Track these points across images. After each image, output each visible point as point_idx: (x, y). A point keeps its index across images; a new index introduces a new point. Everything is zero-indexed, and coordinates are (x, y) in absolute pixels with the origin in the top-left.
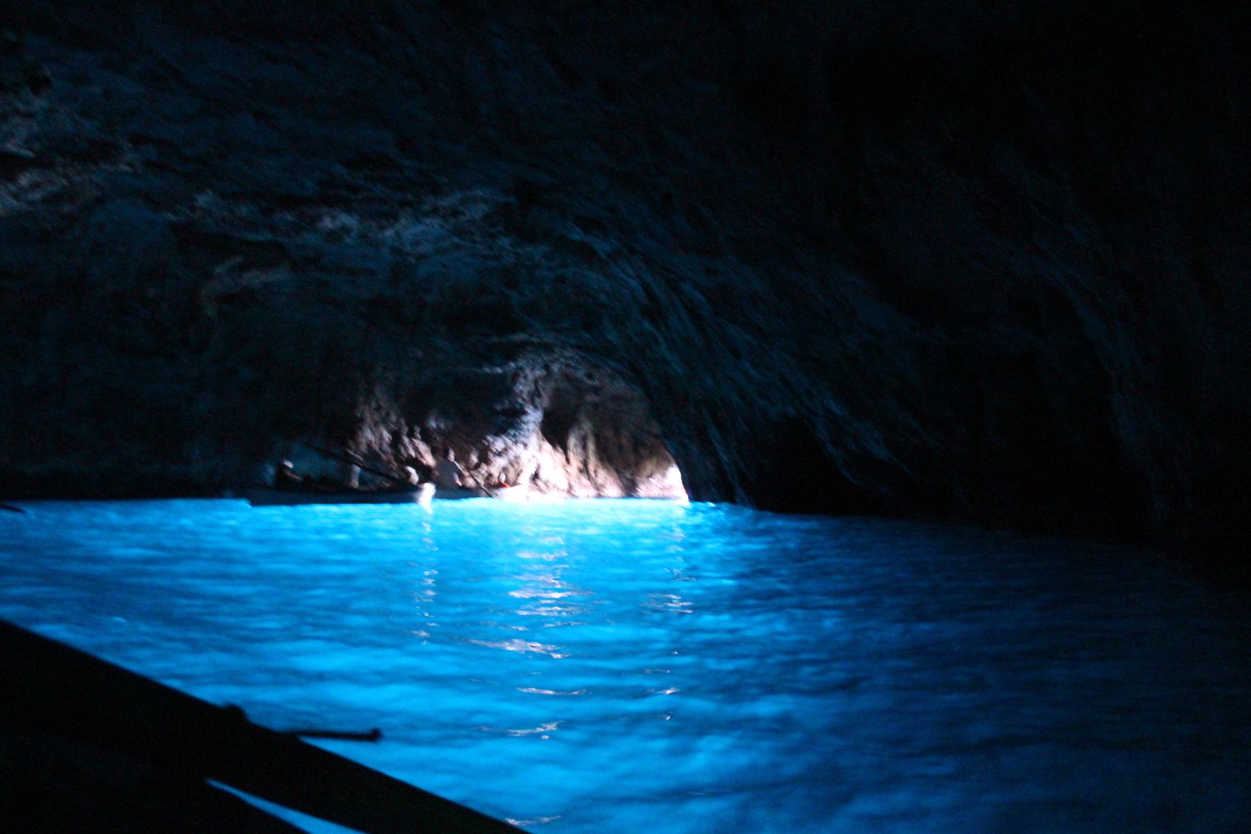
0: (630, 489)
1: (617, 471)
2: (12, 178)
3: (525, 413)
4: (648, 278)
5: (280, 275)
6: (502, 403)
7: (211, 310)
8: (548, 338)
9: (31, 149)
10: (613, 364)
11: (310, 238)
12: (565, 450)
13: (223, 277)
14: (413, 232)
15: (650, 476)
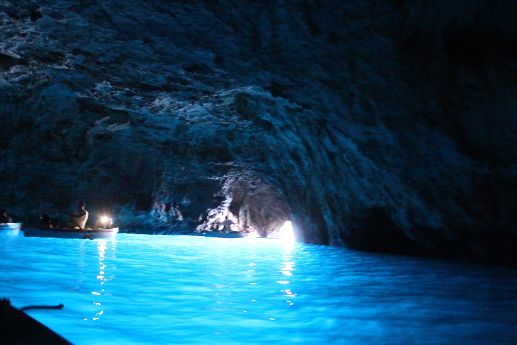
0: (264, 235)
1: (259, 226)
2: (7, 68)
3: (225, 199)
4: (308, 138)
5: (124, 127)
6: (217, 194)
7: (91, 142)
8: (242, 165)
9: (20, 54)
10: (270, 178)
11: (144, 110)
12: (238, 217)
13: (100, 125)
14: (194, 111)
15: (273, 230)
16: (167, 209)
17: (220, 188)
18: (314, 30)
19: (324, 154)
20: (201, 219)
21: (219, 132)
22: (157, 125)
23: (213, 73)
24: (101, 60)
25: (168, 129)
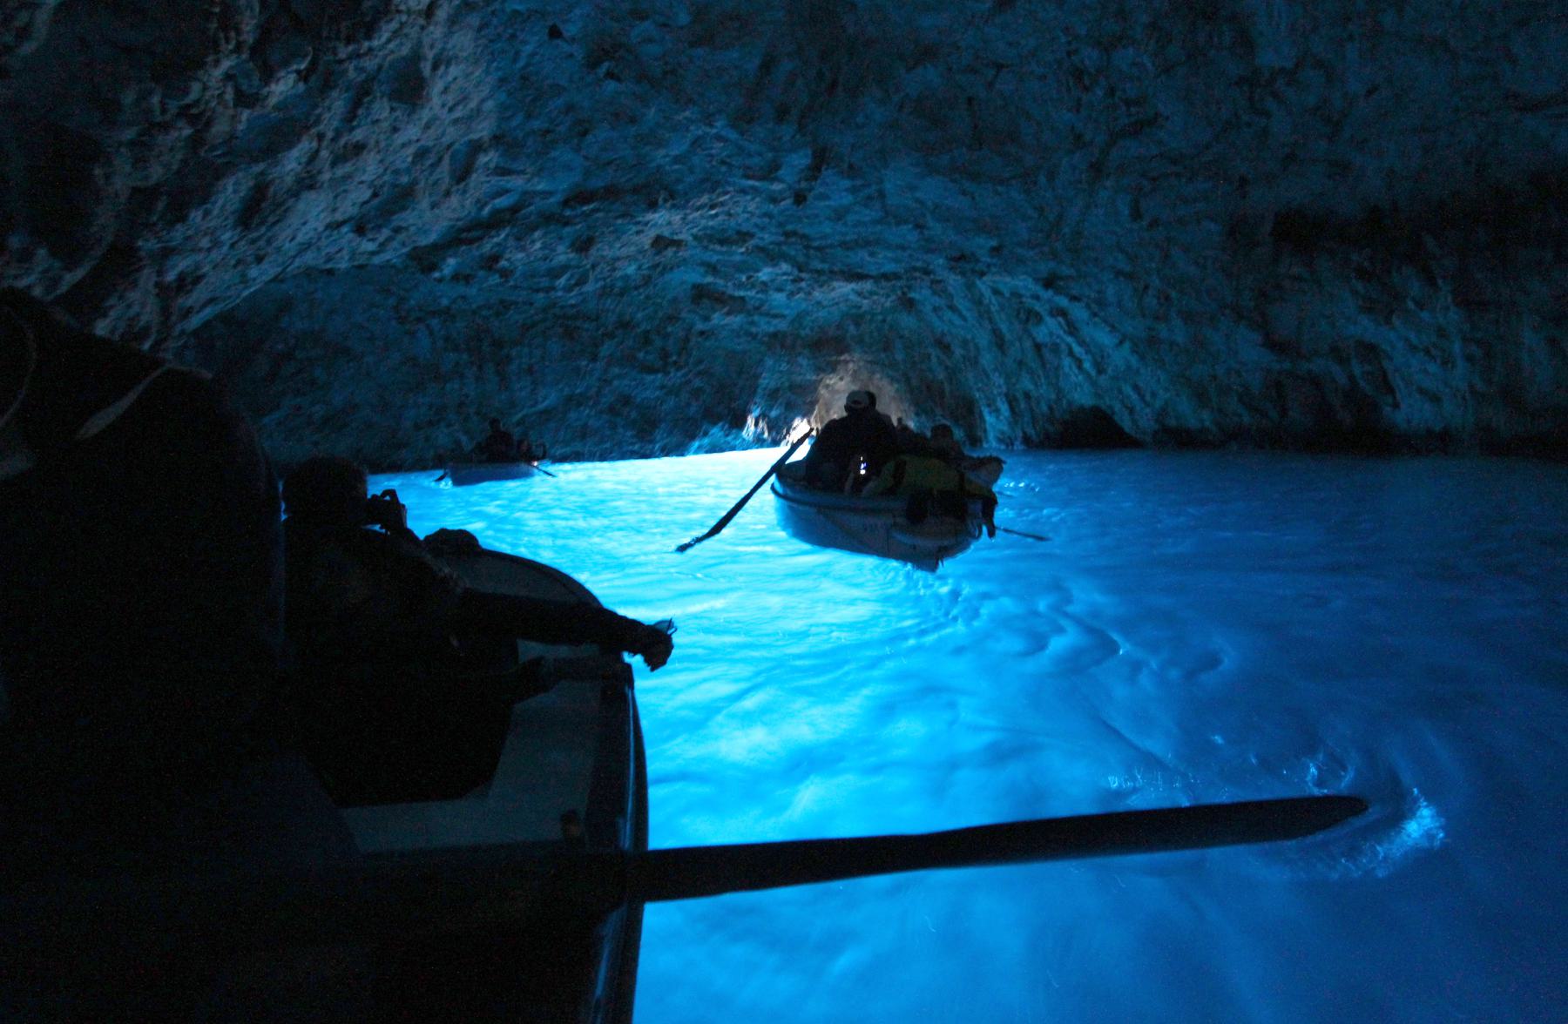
17: (816, 389)
18: (1136, 214)
19: (1028, 344)
22: (773, 312)
25: (783, 316)
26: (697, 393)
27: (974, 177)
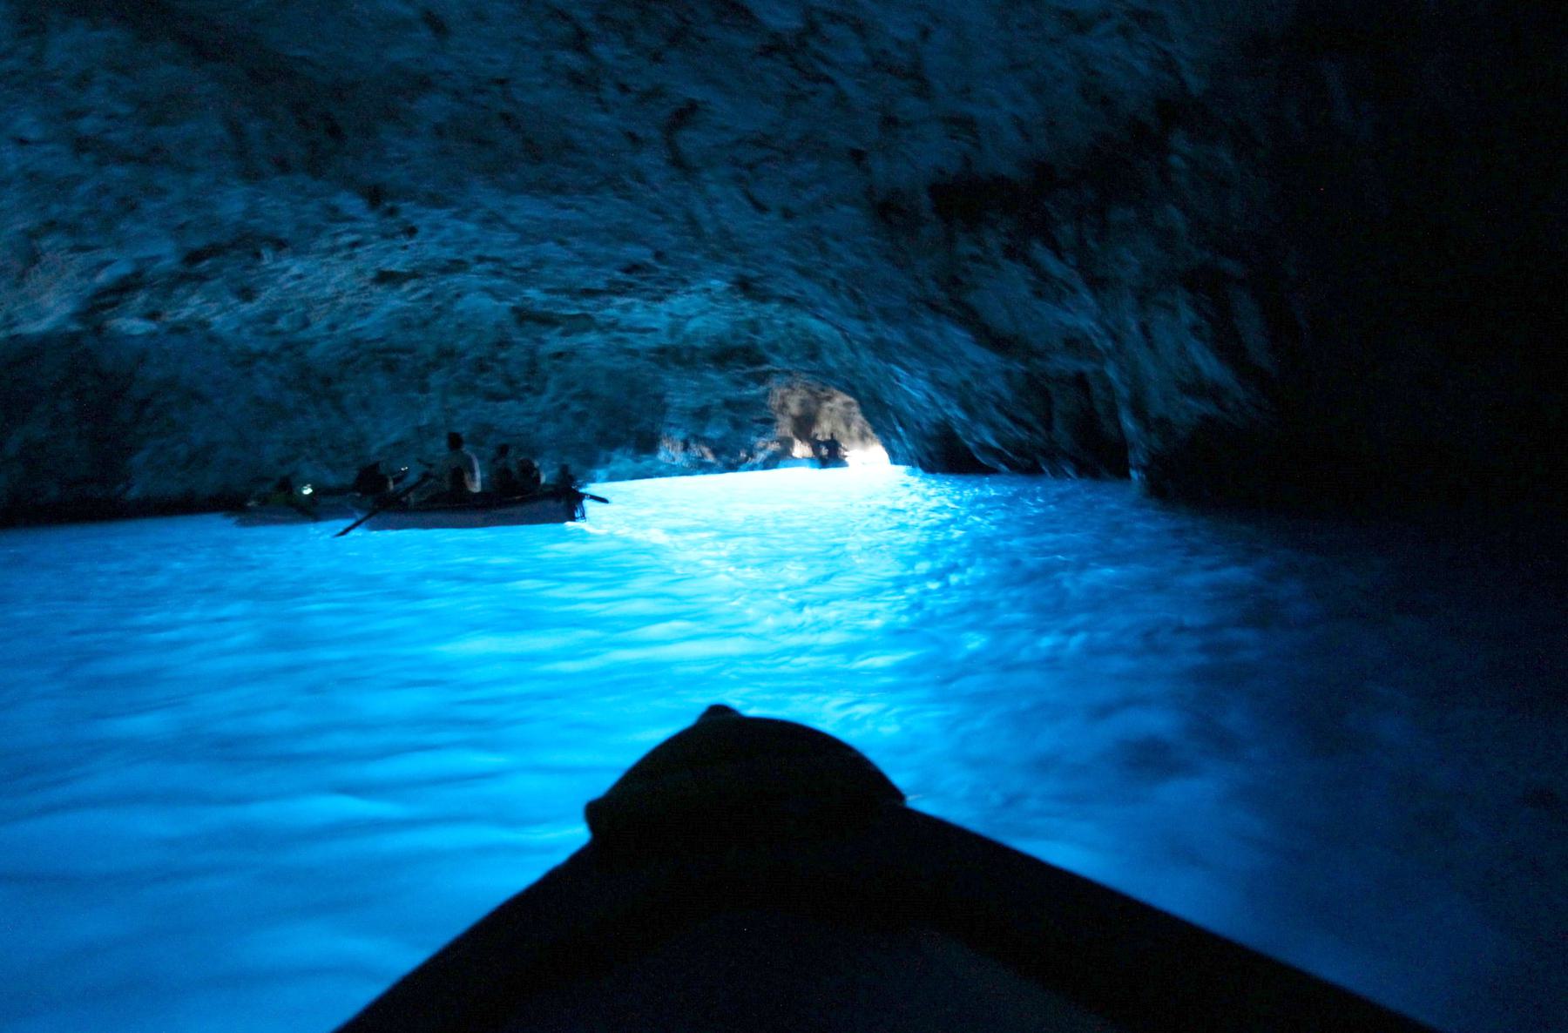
7: (545, 365)
16: (686, 447)
18: (760, 207)
20: (743, 455)
21: (734, 324)
23: (657, 270)
24: (515, 264)
25: (655, 330)
26: (580, 417)
27: (559, 189)
